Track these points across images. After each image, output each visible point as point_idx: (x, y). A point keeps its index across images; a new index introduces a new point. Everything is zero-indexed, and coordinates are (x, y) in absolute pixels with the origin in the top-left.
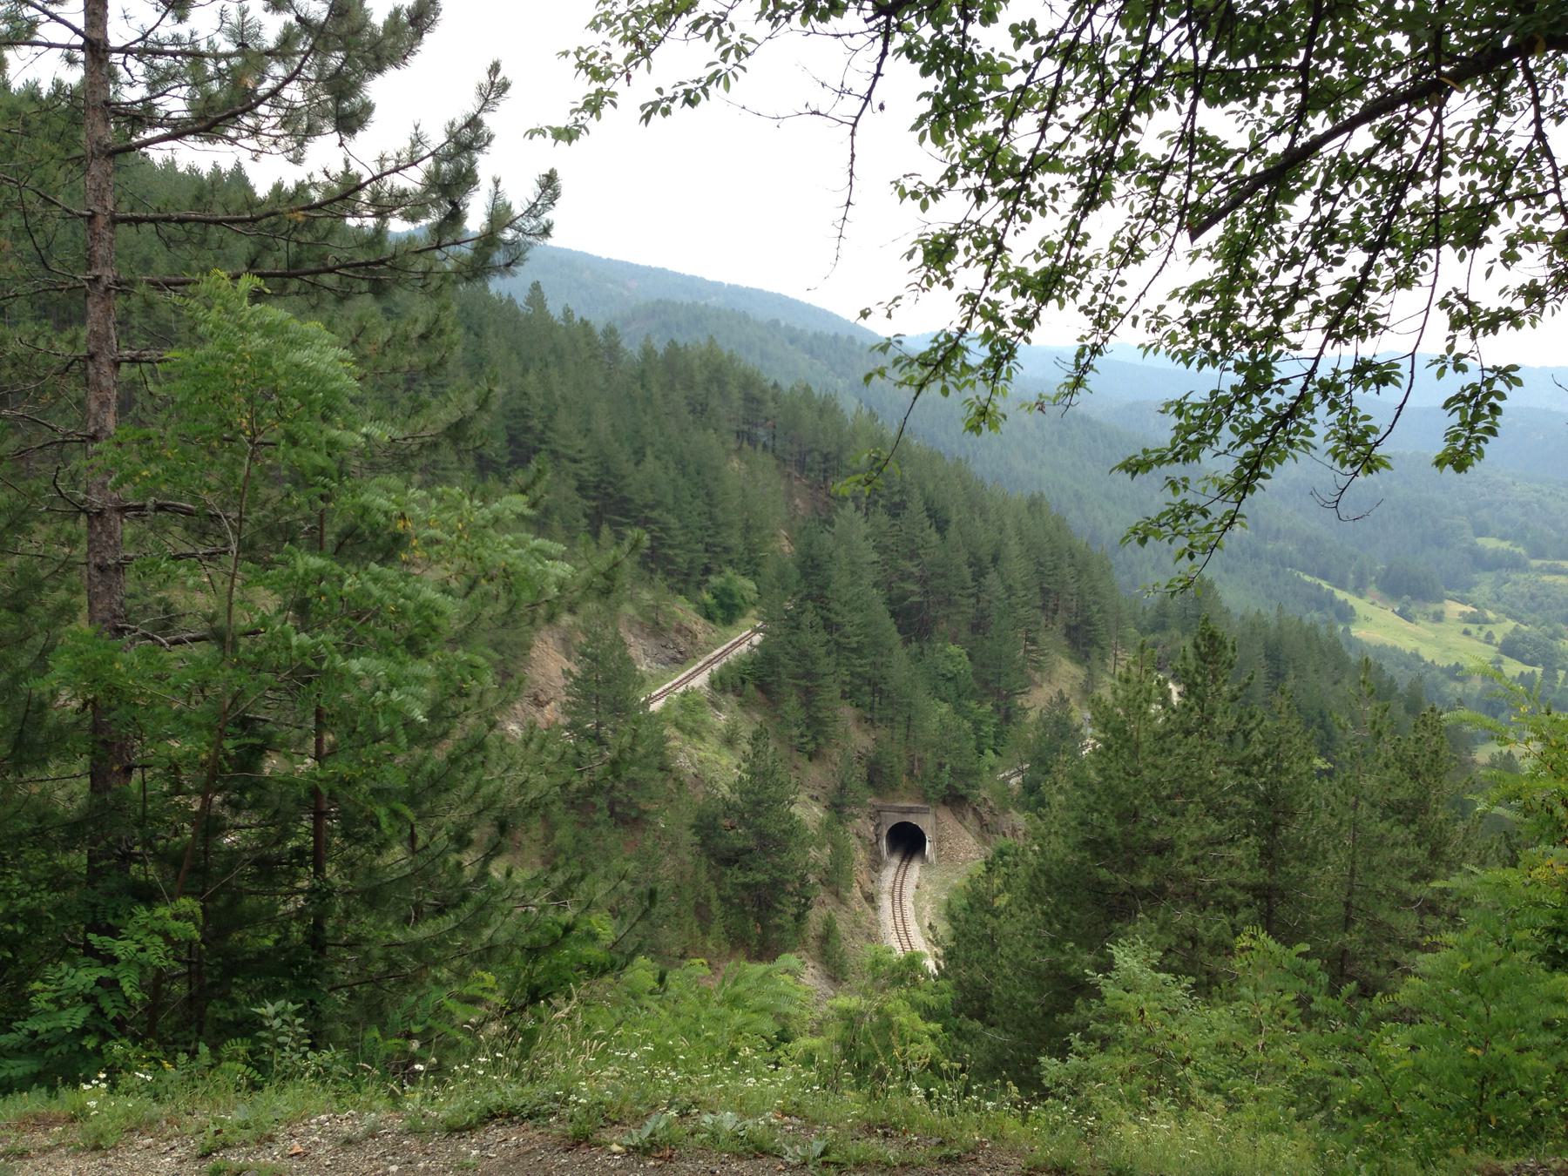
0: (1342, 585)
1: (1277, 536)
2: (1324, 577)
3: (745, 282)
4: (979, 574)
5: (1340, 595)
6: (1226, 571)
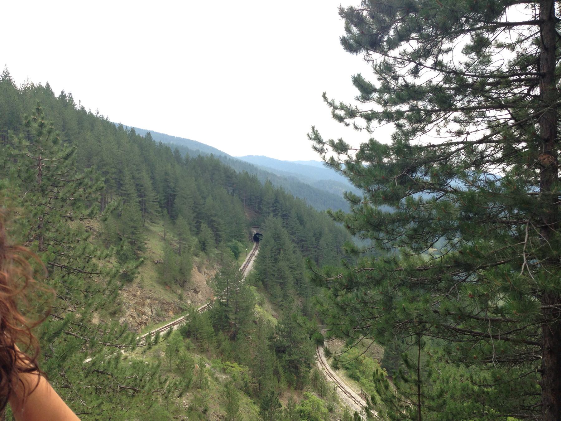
3: (183, 136)
4: (317, 239)
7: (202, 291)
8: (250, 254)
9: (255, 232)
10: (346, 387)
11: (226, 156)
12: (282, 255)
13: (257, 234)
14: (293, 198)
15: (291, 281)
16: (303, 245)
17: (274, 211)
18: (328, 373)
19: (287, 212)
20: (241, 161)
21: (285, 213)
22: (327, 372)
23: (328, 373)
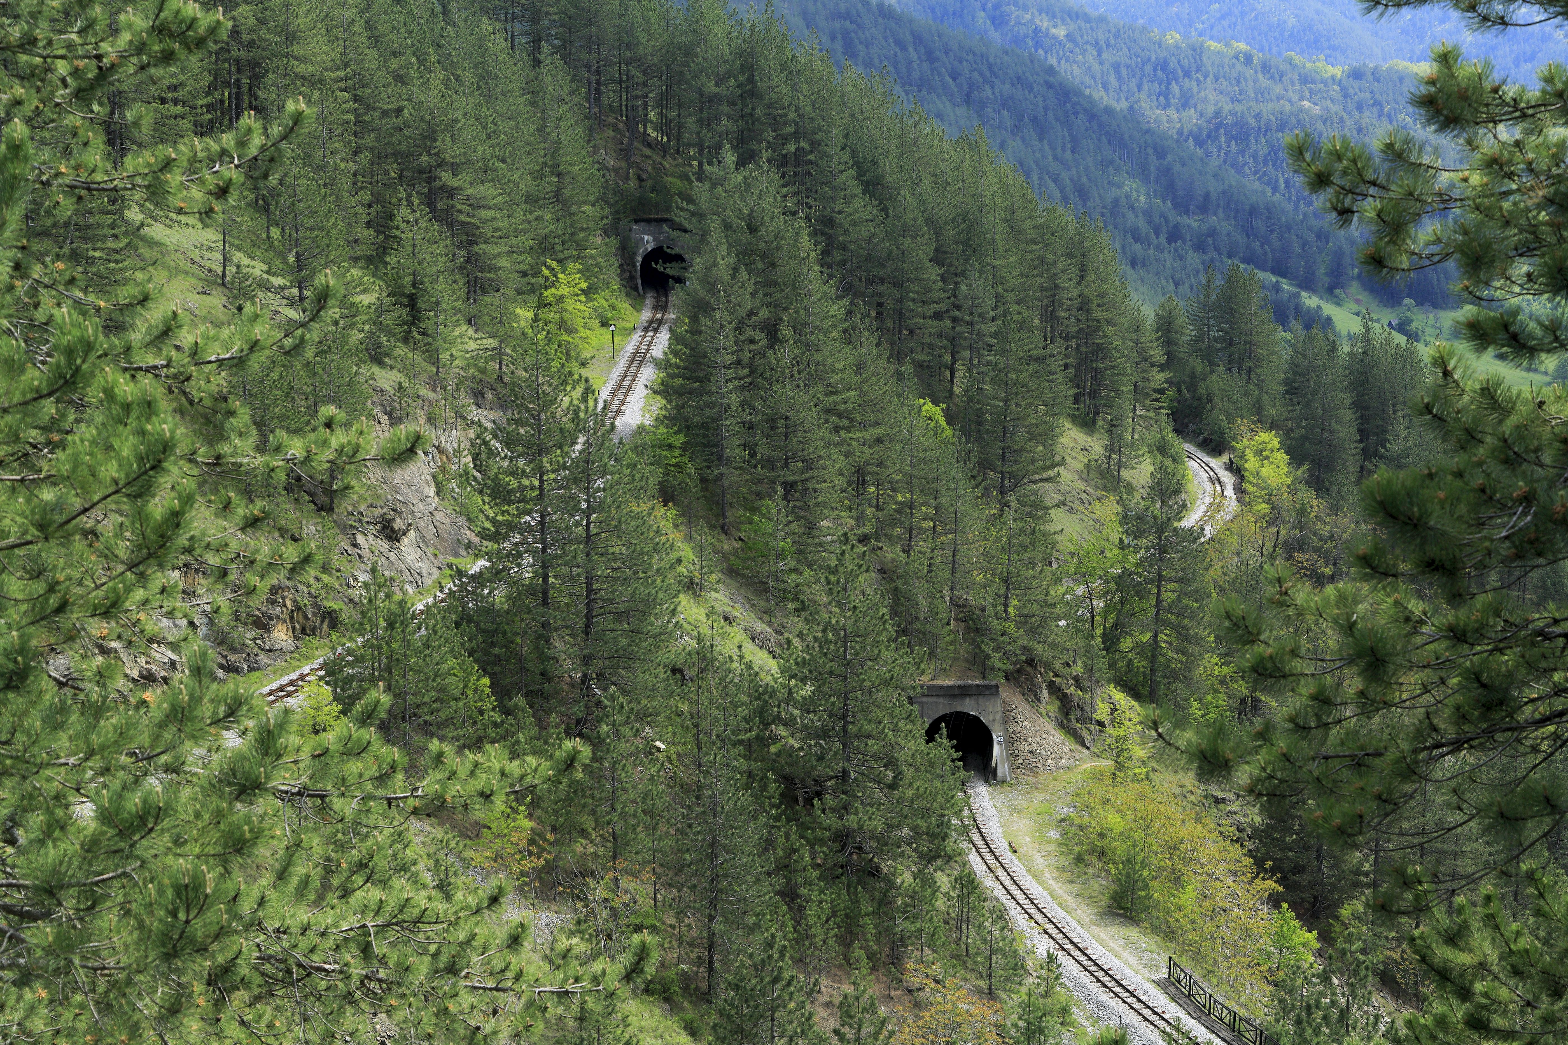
0: (1308, 284)
1: (1204, 208)
2: (1280, 270)
5: (1310, 301)
6: (1133, 263)
9: (648, 242)
10: (1097, 951)
12: (790, 350)
13: (658, 254)
19: (804, 144)
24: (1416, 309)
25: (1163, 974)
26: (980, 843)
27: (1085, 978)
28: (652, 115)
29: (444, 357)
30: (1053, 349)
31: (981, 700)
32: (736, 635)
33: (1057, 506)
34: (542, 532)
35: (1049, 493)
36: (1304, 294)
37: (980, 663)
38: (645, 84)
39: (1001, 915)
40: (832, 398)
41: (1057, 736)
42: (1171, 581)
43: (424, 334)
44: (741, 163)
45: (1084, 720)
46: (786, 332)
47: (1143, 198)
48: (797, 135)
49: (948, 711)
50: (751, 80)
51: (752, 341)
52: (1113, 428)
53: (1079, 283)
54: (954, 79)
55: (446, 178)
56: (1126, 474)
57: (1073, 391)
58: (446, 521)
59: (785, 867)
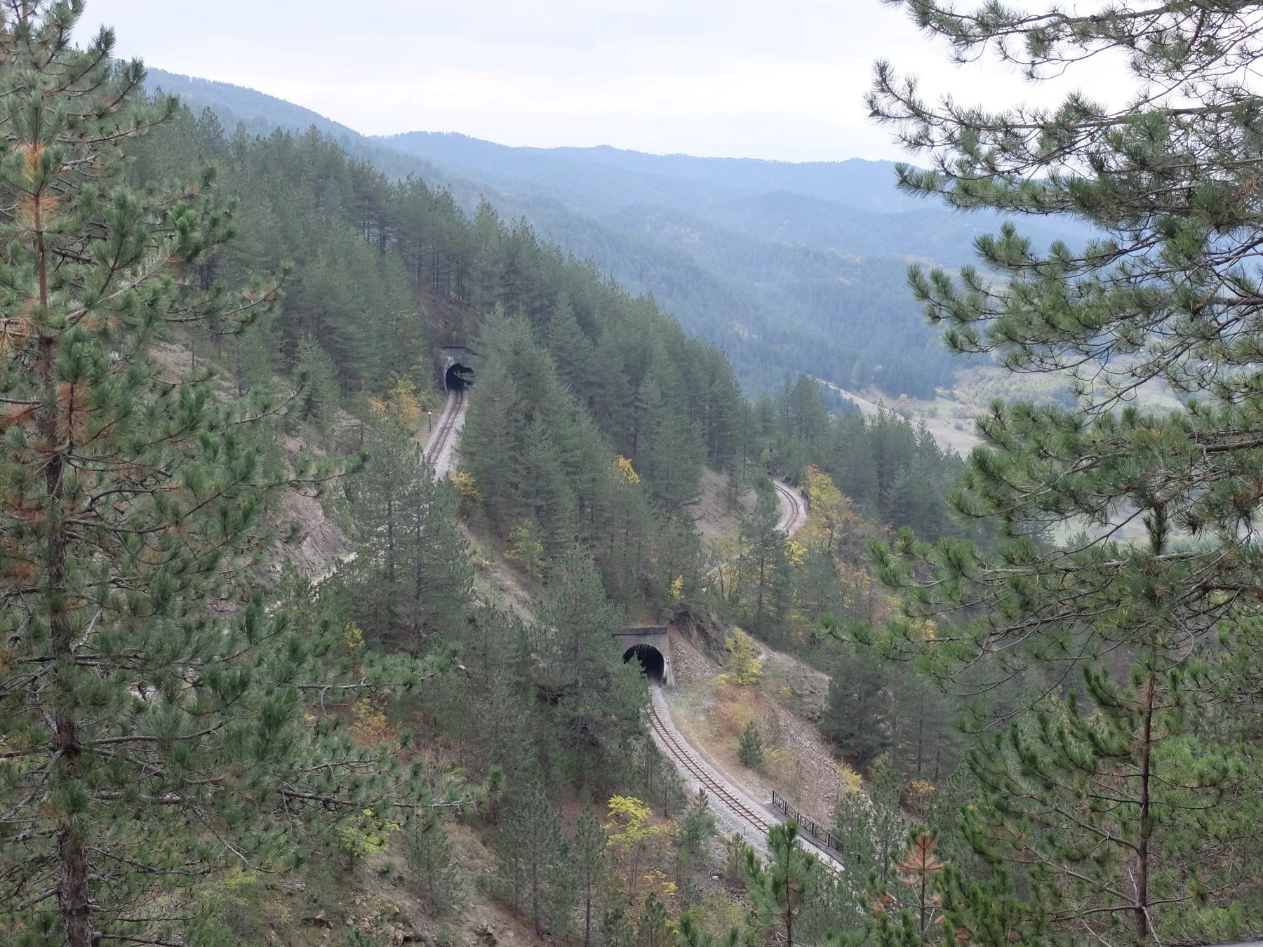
5: (846, 395)
7: (312, 536)
8: (440, 425)
9: (450, 361)
10: (729, 788)
11: (347, 134)
12: (538, 425)
13: (458, 367)
14: (561, 260)
15: (568, 500)
16: (591, 398)
17: (507, 298)
18: (680, 754)
20: (210, 117)
21: (537, 304)
22: (677, 751)
23: (680, 754)
24: (908, 401)
25: (769, 801)
26: (658, 725)
27: (724, 805)
28: (453, 285)
29: (328, 431)
30: (695, 425)
31: (657, 637)
32: (508, 600)
33: (700, 518)
34: (390, 536)
35: (696, 512)
36: (842, 391)
37: (657, 615)
38: (448, 266)
39: (671, 766)
40: (566, 455)
41: (702, 659)
42: (768, 563)
43: (315, 416)
44: (507, 314)
45: (719, 649)
46: (537, 414)
47: (746, 334)
48: (540, 296)
49: (636, 644)
50: (512, 264)
51: (516, 421)
52: (731, 471)
53: (710, 385)
54: (632, 263)
55: (330, 321)
56: (741, 499)
57: (709, 449)
58: (329, 531)
59: (539, 741)
